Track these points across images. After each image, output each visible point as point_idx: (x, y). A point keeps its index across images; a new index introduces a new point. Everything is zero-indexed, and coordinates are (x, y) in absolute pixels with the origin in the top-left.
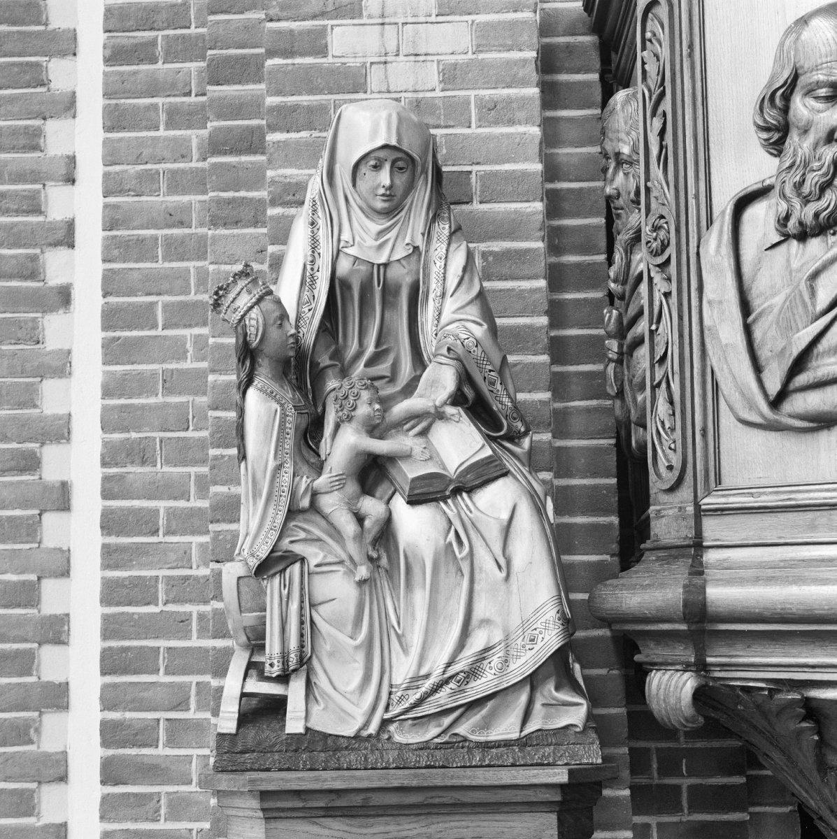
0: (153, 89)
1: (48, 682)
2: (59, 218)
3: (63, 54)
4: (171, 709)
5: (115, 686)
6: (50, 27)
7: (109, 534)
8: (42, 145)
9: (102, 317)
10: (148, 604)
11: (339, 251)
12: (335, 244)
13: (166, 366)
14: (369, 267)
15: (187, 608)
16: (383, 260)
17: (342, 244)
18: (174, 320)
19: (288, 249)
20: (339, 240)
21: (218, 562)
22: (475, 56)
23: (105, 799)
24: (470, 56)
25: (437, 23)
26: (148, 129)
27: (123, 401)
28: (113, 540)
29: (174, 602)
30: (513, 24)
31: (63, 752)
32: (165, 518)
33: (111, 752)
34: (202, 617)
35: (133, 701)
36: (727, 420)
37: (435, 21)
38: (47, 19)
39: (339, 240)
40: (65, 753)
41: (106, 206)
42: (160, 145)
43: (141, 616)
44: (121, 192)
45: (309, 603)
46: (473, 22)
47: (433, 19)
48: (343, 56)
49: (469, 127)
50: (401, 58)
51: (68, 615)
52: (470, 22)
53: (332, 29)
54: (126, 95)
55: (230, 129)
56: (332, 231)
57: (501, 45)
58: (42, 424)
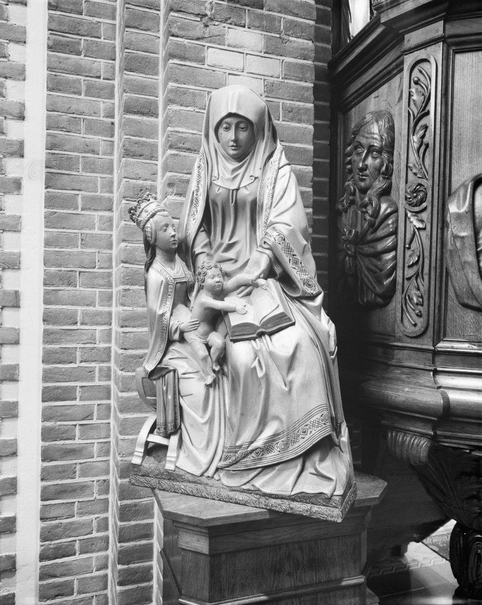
0: (78, 71)
1: (6, 402)
2: (14, 138)
3: (18, 42)
4: (83, 419)
5: (50, 407)
6: (10, 23)
7: (48, 324)
8: (5, 93)
9: (45, 200)
10: (71, 362)
11: (211, 183)
12: (209, 178)
13: (83, 231)
14: (227, 191)
15: (93, 365)
16: (236, 187)
17: (213, 178)
18: (88, 206)
19: (192, 177)
20: (211, 176)
21: (125, 349)
22: (283, 80)
23: (44, 470)
24: (280, 79)
25: (264, 57)
26: (75, 93)
27: (57, 249)
28: (50, 327)
29: (85, 361)
30: (303, 66)
31: (15, 439)
32: (81, 316)
33: (47, 444)
34: (101, 370)
35: (61, 416)
36: (453, 302)
37: (263, 56)
38: (8, 17)
39: (211, 176)
40: (16, 440)
41: (48, 135)
42: (82, 104)
43: (67, 369)
44: (58, 128)
45: (177, 393)
46: (283, 60)
47: (262, 54)
48: (213, 66)
49: (279, 120)
50: (244, 74)
51: (18, 365)
52: (281, 61)
53: (208, 49)
54: (61, 71)
55: (137, 100)
56: (208, 170)
57: (296, 77)
58: (4, 257)
